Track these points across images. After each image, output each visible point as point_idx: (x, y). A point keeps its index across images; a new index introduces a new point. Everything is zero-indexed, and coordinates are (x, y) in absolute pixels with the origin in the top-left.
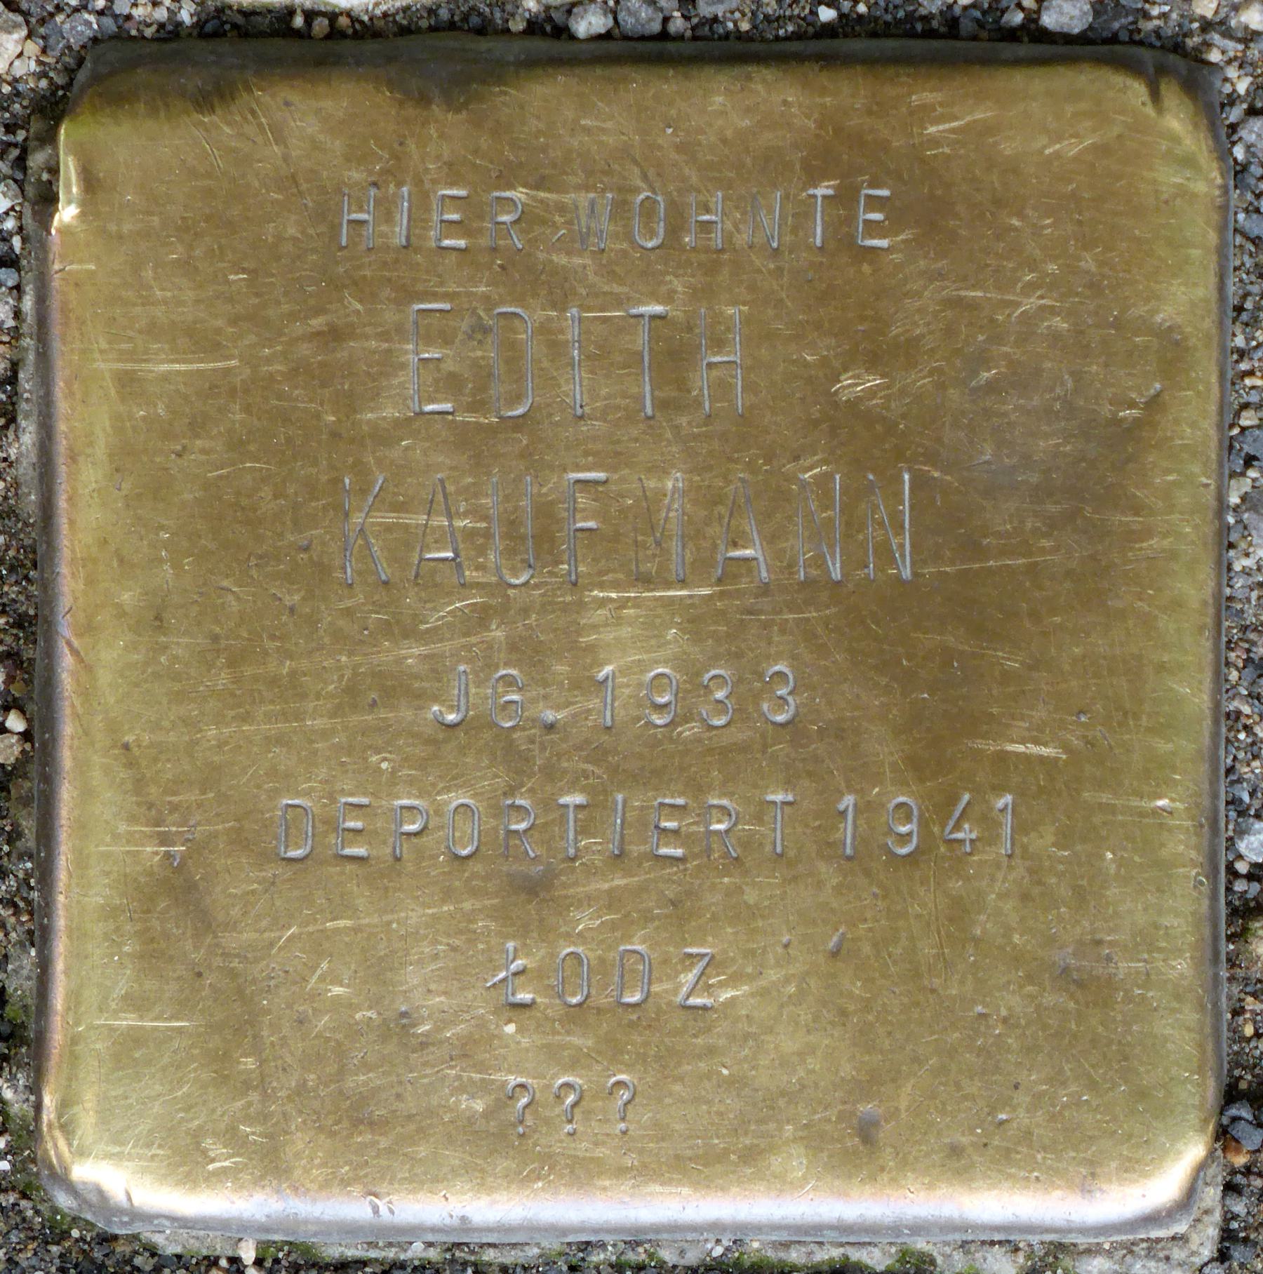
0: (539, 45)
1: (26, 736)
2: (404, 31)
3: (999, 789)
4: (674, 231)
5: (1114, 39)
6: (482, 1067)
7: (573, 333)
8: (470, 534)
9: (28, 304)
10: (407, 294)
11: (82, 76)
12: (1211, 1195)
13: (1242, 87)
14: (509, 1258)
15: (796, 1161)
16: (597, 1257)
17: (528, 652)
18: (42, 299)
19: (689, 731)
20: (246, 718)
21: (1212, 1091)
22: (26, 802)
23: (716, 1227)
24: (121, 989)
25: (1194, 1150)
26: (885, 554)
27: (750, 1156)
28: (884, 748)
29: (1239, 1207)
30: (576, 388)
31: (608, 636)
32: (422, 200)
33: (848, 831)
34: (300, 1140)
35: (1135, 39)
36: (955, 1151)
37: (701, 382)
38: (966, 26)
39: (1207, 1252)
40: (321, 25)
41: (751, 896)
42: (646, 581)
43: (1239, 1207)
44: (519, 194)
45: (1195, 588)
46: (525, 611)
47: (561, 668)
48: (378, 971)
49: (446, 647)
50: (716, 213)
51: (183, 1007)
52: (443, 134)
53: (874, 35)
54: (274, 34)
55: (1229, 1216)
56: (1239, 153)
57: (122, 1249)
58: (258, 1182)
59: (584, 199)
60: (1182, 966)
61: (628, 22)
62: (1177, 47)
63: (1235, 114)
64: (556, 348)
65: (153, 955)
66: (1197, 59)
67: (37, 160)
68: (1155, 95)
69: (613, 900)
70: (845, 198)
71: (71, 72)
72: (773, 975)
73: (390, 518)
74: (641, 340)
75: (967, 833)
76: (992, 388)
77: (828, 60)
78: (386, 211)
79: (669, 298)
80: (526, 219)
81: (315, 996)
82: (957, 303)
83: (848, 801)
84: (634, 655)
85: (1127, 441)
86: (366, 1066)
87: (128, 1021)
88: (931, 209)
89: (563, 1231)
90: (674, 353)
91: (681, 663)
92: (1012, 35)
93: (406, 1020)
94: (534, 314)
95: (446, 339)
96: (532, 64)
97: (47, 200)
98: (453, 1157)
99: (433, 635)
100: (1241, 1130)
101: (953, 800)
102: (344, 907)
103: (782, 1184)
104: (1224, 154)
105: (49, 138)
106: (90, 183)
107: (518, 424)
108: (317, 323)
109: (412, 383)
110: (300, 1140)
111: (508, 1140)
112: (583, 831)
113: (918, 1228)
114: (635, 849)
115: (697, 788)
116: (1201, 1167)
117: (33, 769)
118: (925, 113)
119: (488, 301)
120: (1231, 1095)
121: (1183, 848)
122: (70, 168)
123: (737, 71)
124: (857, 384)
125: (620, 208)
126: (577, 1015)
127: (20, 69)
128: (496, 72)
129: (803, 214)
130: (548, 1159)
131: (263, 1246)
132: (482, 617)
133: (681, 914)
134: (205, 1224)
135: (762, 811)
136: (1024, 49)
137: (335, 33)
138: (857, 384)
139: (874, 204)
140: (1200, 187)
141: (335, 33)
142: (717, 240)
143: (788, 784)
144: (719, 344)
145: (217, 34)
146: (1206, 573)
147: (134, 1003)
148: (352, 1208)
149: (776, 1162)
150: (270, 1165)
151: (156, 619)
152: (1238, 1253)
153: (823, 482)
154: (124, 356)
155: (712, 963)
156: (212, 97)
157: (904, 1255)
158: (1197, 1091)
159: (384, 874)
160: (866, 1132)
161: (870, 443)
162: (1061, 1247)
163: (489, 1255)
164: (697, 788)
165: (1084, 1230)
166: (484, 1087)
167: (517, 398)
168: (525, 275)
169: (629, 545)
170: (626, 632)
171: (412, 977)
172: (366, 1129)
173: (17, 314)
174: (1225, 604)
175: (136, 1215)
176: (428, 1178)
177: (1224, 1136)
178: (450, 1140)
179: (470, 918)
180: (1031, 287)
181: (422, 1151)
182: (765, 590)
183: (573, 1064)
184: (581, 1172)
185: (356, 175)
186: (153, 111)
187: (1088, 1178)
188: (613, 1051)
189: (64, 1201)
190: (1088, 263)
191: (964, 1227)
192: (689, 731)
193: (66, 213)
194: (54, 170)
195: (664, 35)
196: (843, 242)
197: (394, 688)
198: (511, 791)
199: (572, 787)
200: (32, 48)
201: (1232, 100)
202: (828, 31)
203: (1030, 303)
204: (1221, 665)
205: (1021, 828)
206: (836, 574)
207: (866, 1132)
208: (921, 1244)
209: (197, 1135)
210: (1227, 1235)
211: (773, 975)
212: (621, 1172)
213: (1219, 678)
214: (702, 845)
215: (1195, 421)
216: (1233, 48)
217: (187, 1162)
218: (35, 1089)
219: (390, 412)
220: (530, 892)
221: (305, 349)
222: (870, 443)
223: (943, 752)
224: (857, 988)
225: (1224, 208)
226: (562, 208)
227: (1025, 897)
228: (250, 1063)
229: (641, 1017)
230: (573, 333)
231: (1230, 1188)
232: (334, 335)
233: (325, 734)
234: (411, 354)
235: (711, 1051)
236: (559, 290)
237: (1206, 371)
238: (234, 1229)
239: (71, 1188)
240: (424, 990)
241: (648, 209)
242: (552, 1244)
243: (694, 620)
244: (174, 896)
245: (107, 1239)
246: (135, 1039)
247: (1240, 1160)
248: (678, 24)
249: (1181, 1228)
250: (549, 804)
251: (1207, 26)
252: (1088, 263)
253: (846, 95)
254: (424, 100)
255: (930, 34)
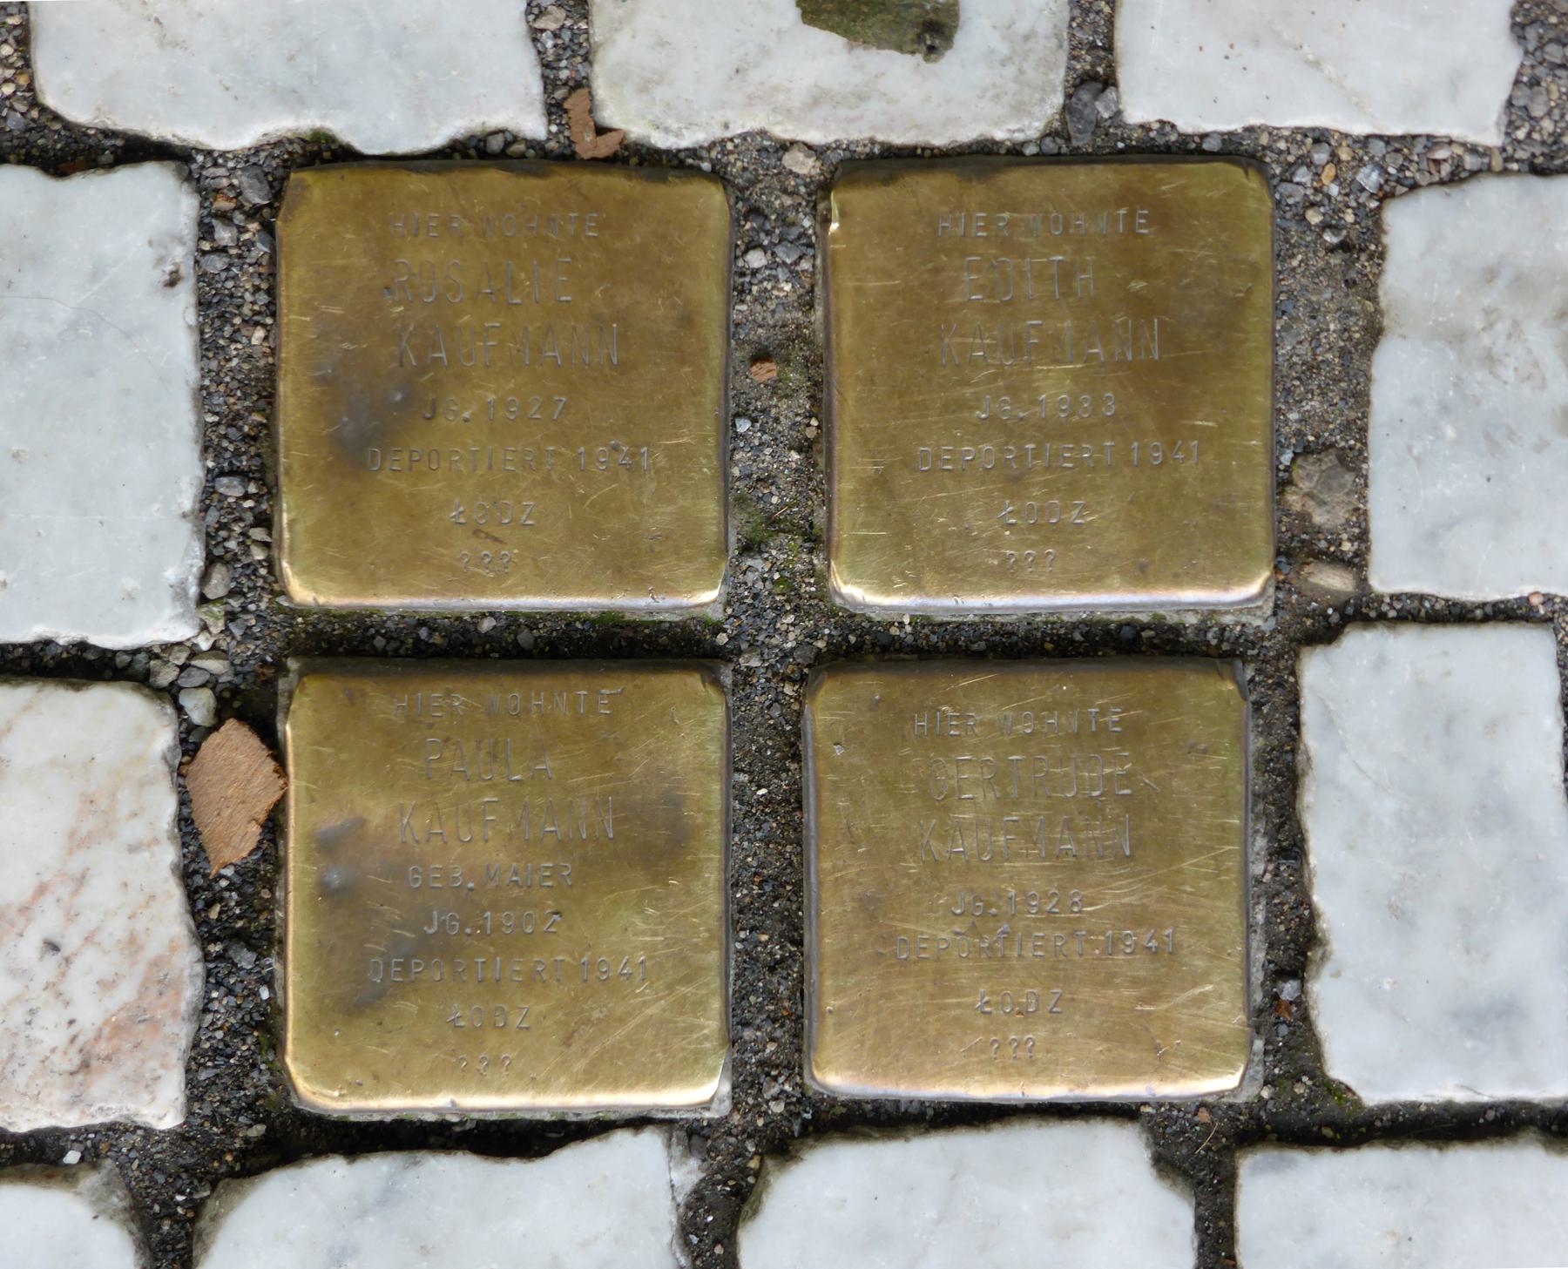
0: (1012, 158)
1: (818, 427)
2: (959, 154)
3: (1193, 439)
4: (1066, 229)
5: (1230, 153)
6: (997, 547)
7: (1027, 268)
8: (989, 346)
9: (819, 261)
10: (964, 254)
11: (838, 174)
12: (1271, 590)
13: (1278, 171)
14: (1004, 620)
15: (1116, 580)
16: (1039, 619)
17: (1013, 391)
18: (824, 260)
19: (1075, 419)
20: (905, 418)
21: (1271, 551)
22: (820, 452)
23: (1085, 606)
24: (860, 520)
25: (1266, 574)
26: (1148, 350)
27: (1099, 579)
28: (1149, 424)
29: (1281, 595)
30: (1029, 288)
31: (1041, 384)
32: (969, 218)
33: (1135, 456)
34: (928, 576)
35: (1238, 153)
36: (1176, 575)
37: (1077, 285)
38: (1174, 149)
39: (1269, 612)
40: (928, 153)
41: (1099, 481)
42: (1057, 362)
43: (1281, 595)
44: (1006, 215)
45: (1264, 361)
46: (1011, 374)
47: (1025, 396)
48: (957, 512)
49: (980, 389)
50: (1081, 221)
51: (883, 527)
52: (978, 192)
53: (264, 479)
54: (909, 156)
55: (1277, 599)
56: (1277, 196)
57: (857, 619)
58: (912, 592)
59: (1031, 216)
60: (1261, 504)
61: (1045, 149)
62: (1253, 156)
63: (1275, 182)
64: (1022, 274)
65: (872, 507)
66: (1261, 161)
67: (821, 206)
68: (1246, 173)
69: (1046, 484)
70: (1131, 215)
71: (833, 173)
72: (1107, 511)
73: (959, 340)
74: (1054, 270)
75: (1180, 456)
76: (1188, 286)
77: (1123, 162)
78: (955, 222)
79: (1063, 254)
80: (1010, 224)
81: (933, 522)
82: (1175, 254)
83: (1136, 444)
84: (1054, 387)
85: (1238, 306)
86: (952, 548)
87: (863, 532)
88: (1164, 216)
89: (1028, 608)
90: (1067, 274)
91: (1070, 393)
92: (1191, 152)
93: (969, 530)
94: (1011, 261)
95: (979, 271)
96: (1010, 165)
97: (827, 221)
98: (986, 582)
99: (977, 385)
100: (1282, 566)
101: (1175, 443)
102: (943, 489)
103: (1111, 589)
104: (1272, 196)
105: (828, 198)
106: (843, 215)
107: (1008, 303)
108: (930, 266)
109: (967, 289)
110: (928, 576)
111: (1008, 576)
112: (1034, 458)
113: (1162, 605)
114: (1054, 465)
115: (1077, 441)
116: (1268, 580)
117: (823, 440)
118: (1162, 182)
119: (996, 257)
120: (1278, 553)
121: (1261, 458)
122: (835, 212)
123: (1089, 167)
124: (1138, 285)
125: (1046, 219)
126: (1033, 528)
127: (813, 172)
128: (997, 169)
129: (1115, 220)
130: (1022, 581)
131: (912, 617)
132: (994, 378)
133: (1072, 489)
134: (891, 608)
135: (1102, 449)
136: (1196, 157)
137: (933, 156)
138: (1138, 285)
139: (1142, 216)
140: (1264, 208)
141: (933, 156)
142: (1082, 231)
143: (1112, 439)
144: (1084, 271)
145: (888, 157)
146: (1269, 355)
147: (865, 525)
148: (948, 601)
149: (1108, 581)
150: (916, 585)
151: (870, 380)
152: (1280, 613)
153: (1125, 323)
154: (858, 280)
155: (1085, 507)
156: (888, 180)
157: (1155, 616)
158: (1266, 549)
159: (958, 476)
160: (1143, 569)
161: (1142, 307)
162: (1214, 612)
163: (998, 619)
164: (1077, 441)
165: (1224, 604)
166: (997, 555)
167: (1006, 294)
168: (1008, 245)
169: (1052, 349)
170: (1049, 382)
171: (970, 514)
172: (956, 574)
173: (814, 266)
174: (1275, 367)
175: (867, 606)
176: (977, 589)
177: (1277, 569)
178: (985, 575)
179: (991, 491)
180: (1203, 247)
181: (975, 579)
182: (1102, 365)
183: (1031, 546)
184: (1034, 587)
185: (944, 209)
186: (867, 186)
187: (1226, 586)
188: (1047, 541)
189: (838, 601)
190: (1223, 237)
191: (1179, 604)
192: (1075, 419)
193: (834, 226)
194: (829, 210)
195: (1059, 154)
196: (1131, 229)
197: (962, 405)
198: (1007, 444)
199: (1030, 442)
200: (818, 164)
201: (1274, 176)
202: (1121, 151)
203: (1202, 253)
204: (1274, 390)
205: (1201, 453)
206: (1130, 357)
207: (1143, 569)
208: (1161, 612)
209: (890, 575)
210: (1276, 606)
211: (1107, 511)
212: (1050, 586)
213: (1274, 396)
214: (1079, 462)
215: (1263, 297)
216: (1274, 156)
217: (886, 586)
218: (828, 559)
219: (958, 300)
220: (1015, 481)
221: (926, 276)
222: (1142, 307)
223: (1171, 426)
224: (1139, 515)
225: (1273, 217)
226: (1022, 220)
227: (1202, 480)
228: (909, 547)
229: (1059, 527)
230: (1027, 268)
231: (1278, 588)
232: (937, 270)
233: (936, 423)
234: (966, 276)
235: (1083, 540)
236: (1022, 252)
237: (1269, 278)
238: (901, 610)
239: (841, 595)
240: (974, 519)
241: (1056, 220)
242: (1021, 614)
243: (1076, 376)
244: (880, 486)
245: (852, 616)
246: (866, 539)
247: (1281, 577)
248: (1064, 150)
249: (1260, 603)
250: (1021, 448)
251: (1264, 148)
252: (1223, 237)
253: (1130, 174)
254: (969, 180)
255: (1160, 152)
